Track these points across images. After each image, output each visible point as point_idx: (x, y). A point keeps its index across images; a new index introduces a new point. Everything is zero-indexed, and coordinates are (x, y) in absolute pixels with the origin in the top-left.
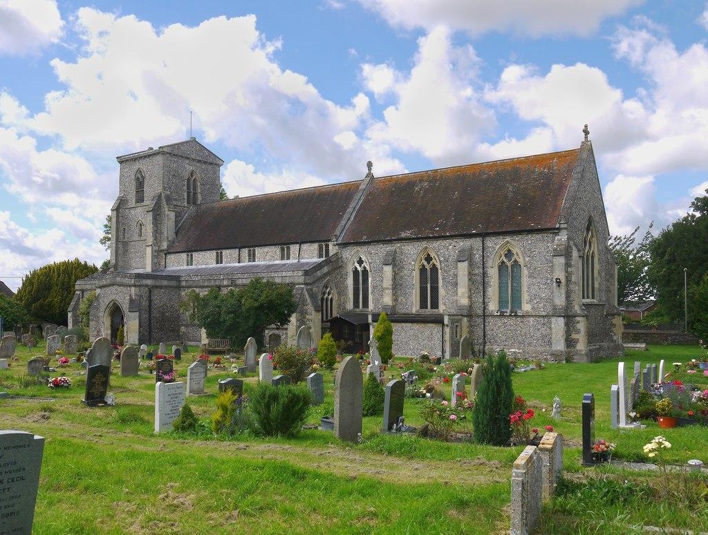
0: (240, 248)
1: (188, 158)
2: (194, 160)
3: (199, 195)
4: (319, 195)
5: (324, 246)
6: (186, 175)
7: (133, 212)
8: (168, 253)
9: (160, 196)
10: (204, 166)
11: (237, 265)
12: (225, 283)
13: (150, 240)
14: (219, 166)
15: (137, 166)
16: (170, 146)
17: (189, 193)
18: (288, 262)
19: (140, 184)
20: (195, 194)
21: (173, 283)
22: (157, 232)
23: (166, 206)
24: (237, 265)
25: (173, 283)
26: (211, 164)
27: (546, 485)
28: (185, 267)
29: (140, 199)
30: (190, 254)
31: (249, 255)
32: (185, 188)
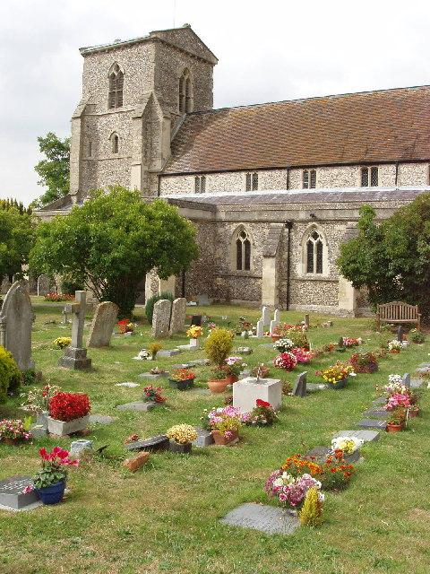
0: (289, 169)
1: (181, 51)
2: (187, 53)
3: (192, 101)
4: (289, 111)
5: (369, 172)
6: (179, 72)
7: (103, 121)
8: (162, 175)
9: (151, 98)
10: (197, 64)
11: (284, 192)
12: (302, 216)
13: (138, 157)
14: (212, 64)
15: (107, 61)
16: (165, 31)
17: (181, 97)
18: (312, 191)
19: (116, 81)
20: (187, 98)
21: (208, 215)
22: (148, 148)
23: (158, 107)
24: (284, 192)
25: (208, 215)
26: (205, 61)
27: (65, 339)
28: (244, 193)
29: (116, 99)
30: (200, 177)
31: (305, 178)
32: (177, 90)
